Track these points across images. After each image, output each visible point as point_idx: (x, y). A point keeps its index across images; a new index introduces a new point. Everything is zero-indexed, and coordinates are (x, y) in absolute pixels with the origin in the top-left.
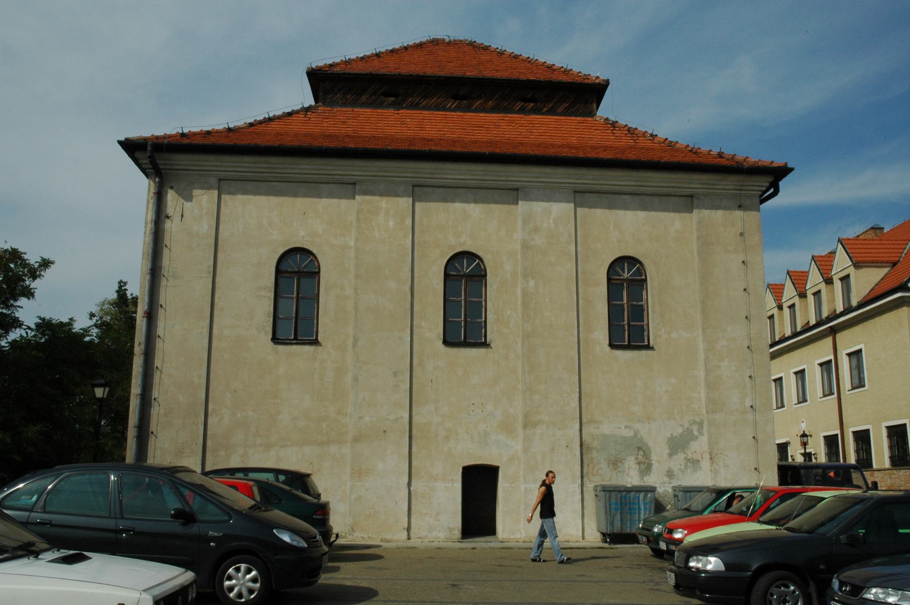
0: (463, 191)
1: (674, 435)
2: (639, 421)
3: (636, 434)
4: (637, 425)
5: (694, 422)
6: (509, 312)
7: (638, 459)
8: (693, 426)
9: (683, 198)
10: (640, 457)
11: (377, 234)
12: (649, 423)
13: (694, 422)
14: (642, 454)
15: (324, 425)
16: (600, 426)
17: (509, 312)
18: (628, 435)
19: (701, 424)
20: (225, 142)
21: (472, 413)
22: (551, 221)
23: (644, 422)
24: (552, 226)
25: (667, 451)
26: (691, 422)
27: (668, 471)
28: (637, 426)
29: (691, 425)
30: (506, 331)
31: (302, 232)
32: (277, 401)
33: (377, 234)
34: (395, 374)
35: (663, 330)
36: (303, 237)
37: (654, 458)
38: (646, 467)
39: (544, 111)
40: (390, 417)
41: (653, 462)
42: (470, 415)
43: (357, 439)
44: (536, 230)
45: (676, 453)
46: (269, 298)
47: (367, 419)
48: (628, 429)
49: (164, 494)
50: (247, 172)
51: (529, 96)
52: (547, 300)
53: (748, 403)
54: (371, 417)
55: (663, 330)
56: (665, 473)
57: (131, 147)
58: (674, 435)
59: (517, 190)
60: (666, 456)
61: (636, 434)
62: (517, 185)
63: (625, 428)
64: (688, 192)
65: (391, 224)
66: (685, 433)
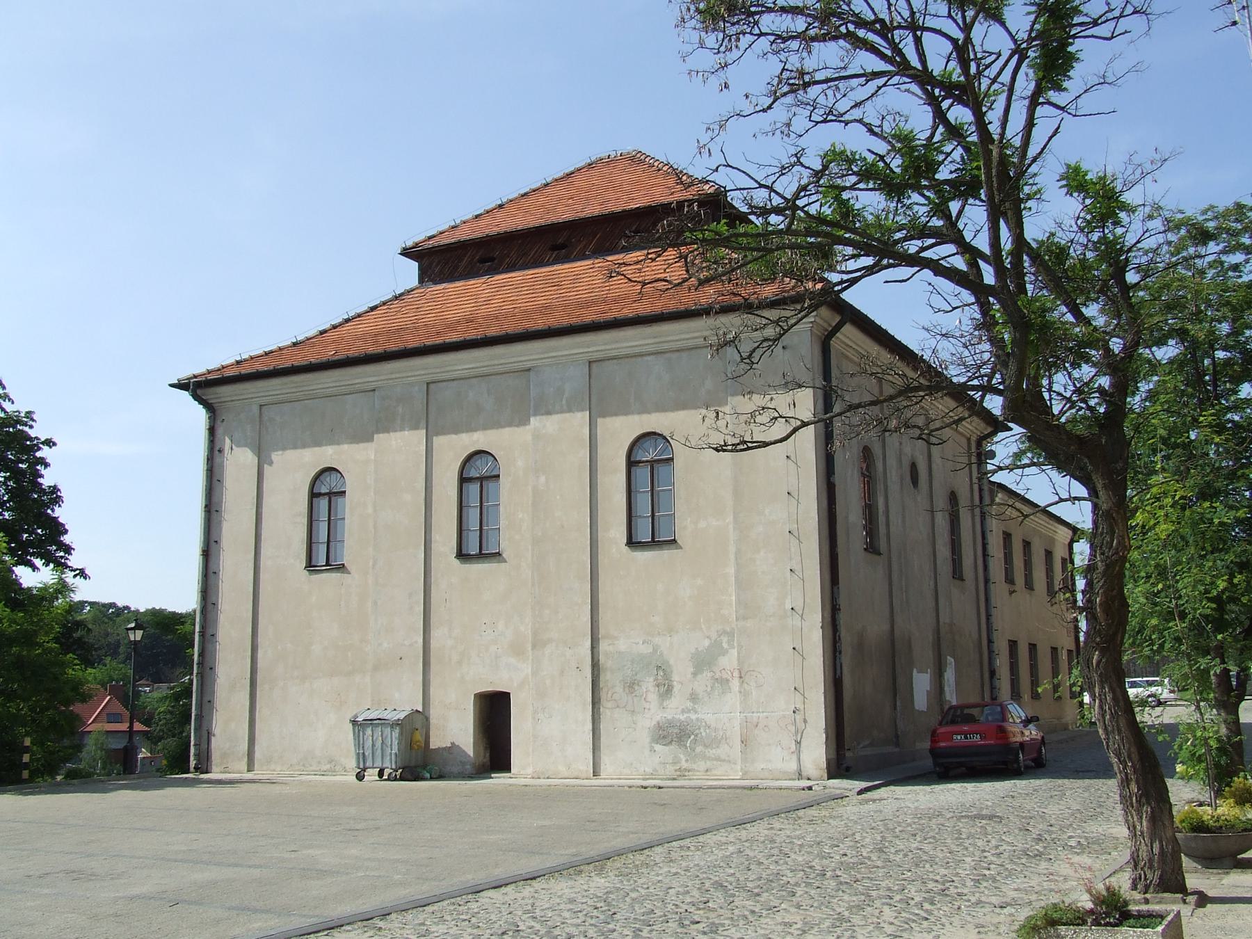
0: (474, 380)
2: (659, 634)
3: (655, 651)
6: (520, 516)
7: (657, 680)
10: (660, 677)
13: (725, 632)
15: (349, 654)
16: (616, 642)
22: (564, 402)
23: (665, 635)
27: (691, 694)
28: (657, 640)
35: (689, 519)
40: (406, 642)
42: (481, 636)
43: (376, 668)
47: (385, 645)
52: (558, 497)
55: (689, 519)
57: (181, 386)
59: (529, 370)
60: (689, 676)
62: (528, 365)
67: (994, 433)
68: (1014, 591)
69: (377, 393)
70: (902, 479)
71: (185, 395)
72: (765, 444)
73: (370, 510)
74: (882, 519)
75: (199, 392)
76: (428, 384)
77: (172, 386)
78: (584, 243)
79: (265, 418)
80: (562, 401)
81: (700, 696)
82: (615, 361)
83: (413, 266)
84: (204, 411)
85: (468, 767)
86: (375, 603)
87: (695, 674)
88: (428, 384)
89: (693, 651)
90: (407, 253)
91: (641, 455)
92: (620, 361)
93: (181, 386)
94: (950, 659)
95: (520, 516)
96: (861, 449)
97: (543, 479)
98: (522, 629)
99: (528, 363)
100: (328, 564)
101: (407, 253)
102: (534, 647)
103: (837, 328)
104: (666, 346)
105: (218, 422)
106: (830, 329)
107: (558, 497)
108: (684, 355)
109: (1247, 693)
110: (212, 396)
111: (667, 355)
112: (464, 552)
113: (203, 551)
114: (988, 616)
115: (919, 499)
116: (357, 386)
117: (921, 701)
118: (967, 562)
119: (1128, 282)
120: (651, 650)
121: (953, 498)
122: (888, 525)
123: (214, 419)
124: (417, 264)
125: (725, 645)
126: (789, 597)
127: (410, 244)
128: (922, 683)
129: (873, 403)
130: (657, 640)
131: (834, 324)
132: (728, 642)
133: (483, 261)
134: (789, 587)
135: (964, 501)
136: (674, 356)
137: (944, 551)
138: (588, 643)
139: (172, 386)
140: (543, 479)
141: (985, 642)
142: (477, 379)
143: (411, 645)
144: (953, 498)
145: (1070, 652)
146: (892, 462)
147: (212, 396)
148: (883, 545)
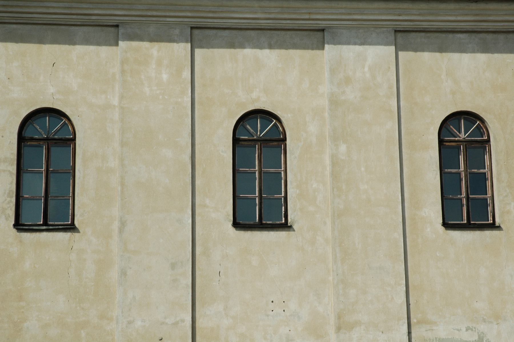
0: (252, 33)
2: (484, 321)
6: (315, 185)
16: (434, 328)
22: (366, 69)
24: (368, 75)
28: (482, 327)
30: (311, 209)
31: (52, 88)
32: (23, 304)
34: (173, 266)
42: (268, 316)
44: (348, 81)
46: (11, 173)
47: (139, 323)
48: (470, 331)
52: (363, 169)
54: (143, 321)
59: (323, 30)
62: (323, 24)
63: (467, 330)
65: (165, 77)
73: (113, 163)
76: (192, 28)
80: (364, 68)
85: (319, 234)
86: (123, 273)
92: (429, 35)
95: (315, 185)
99: (324, 22)
100: (45, 223)
102: (339, 329)
104: (484, 25)
107: (363, 169)
108: (502, 37)
109: (51, 118)
112: (237, 221)
116: (94, 17)
119: (237, 222)
129: (70, 260)
130: (482, 327)
136: (490, 37)
138: (405, 328)
140: (343, 148)
142: (257, 32)
143: (176, 324)
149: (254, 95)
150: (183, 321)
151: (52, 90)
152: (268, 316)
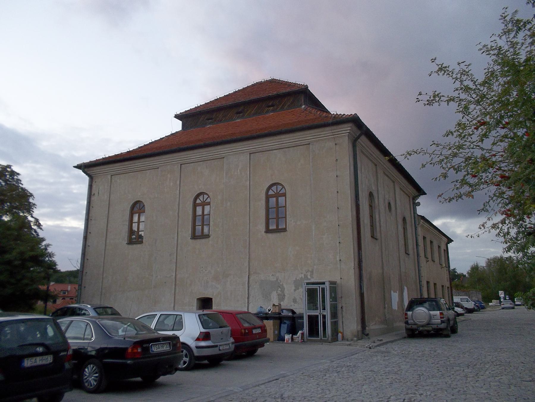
1: (297, 279)
2: (279, 272)
3: (277, 279)
4: (278, 274)
5: (308, 271)
6: (219, 220)
8: (308, 273)
9: (305, 146)
10: (279, 291)
11: (166, 190)
12: (284, 273)
14: (280, 290)
17: (219, 220)
18: (273, 280)
19: (312, 272)
20: (128, 156)
21: (201, 272)
22: (239, 171)
23: (282, 272)
24: (239, 173)
25: (294, 288)
26: (306, 271)
27: (293, 299)
29: (307, 272)
33: (166, 190)
36: (140, 196)
37: (286, 292)
38: (282, 297)
39: (285, 108)
41: (286, 294)
45: (298, 289)
47: (159, 277)
48: (273, 276)
49: (509, 208)
50: (324, 137)
51: (270, 104)
52: (235, 212)
53: (338, 259)
54: (160, 276)
55: (293, 221)
56: (292, 301)
57: (79, 167)
58: (297, 279)
61: (277, 279)
63: (272, 276)
64: (307, 142)
65: (171, 184)
66: (129, 324)
67: (419, 195)
68: (428, 261)
69: (159, 169)
70: (385, 208)
71: (80, 172)
72: (271, 381)
74: (378, 224)
75: (86, 170)
77: (75, 167)
78: (250, 111)
79: (113, 181)
80: (237, 170)
81: (297, 300)
82: (261, 153)
83: (180, 123)
84: (88, 178)
87: (295, 290)
88: (181, 165)
89: (294, 279)
90: (177, 117)
91: (271, 192)
93: (79, 167)
94: (405, 288)
96: (369, 193)
97: (229, 204)
98: (218, 270)
101: (177, 117)
103: (358, 137)
105: (94, 183)
106: (356, 137)
107: (235, 212)
110: (91, 172)
111: (283, 149)
113: (84, 237)
114: (419, 270)
115: (392, 218)
117: (395, 306)
118: (410, 247)
120: (275, 279)
121: (404, 219)
122: (380, 226)
123: (92, 180)
124: (181, 122)
125: (309, 277)
126: (339, 254)
127: (178, 113)
128: (395, 296)
131: (358, 135)
132: (311, 276)
133: (208, 119)
134: (338, 250)
135: (408, 219)
136: (286, 149)
137: (402, 242)
139: (75, 167)
140: (229, 204)
141: (418, 281)
144: (404, 219)
145: (448, 287)
146: (381, 200)
147: (91, 172)
148: (378, 235)
149: (200, 187)
150: (172, 276)
151: (139, 194)
152: (200, 273)
